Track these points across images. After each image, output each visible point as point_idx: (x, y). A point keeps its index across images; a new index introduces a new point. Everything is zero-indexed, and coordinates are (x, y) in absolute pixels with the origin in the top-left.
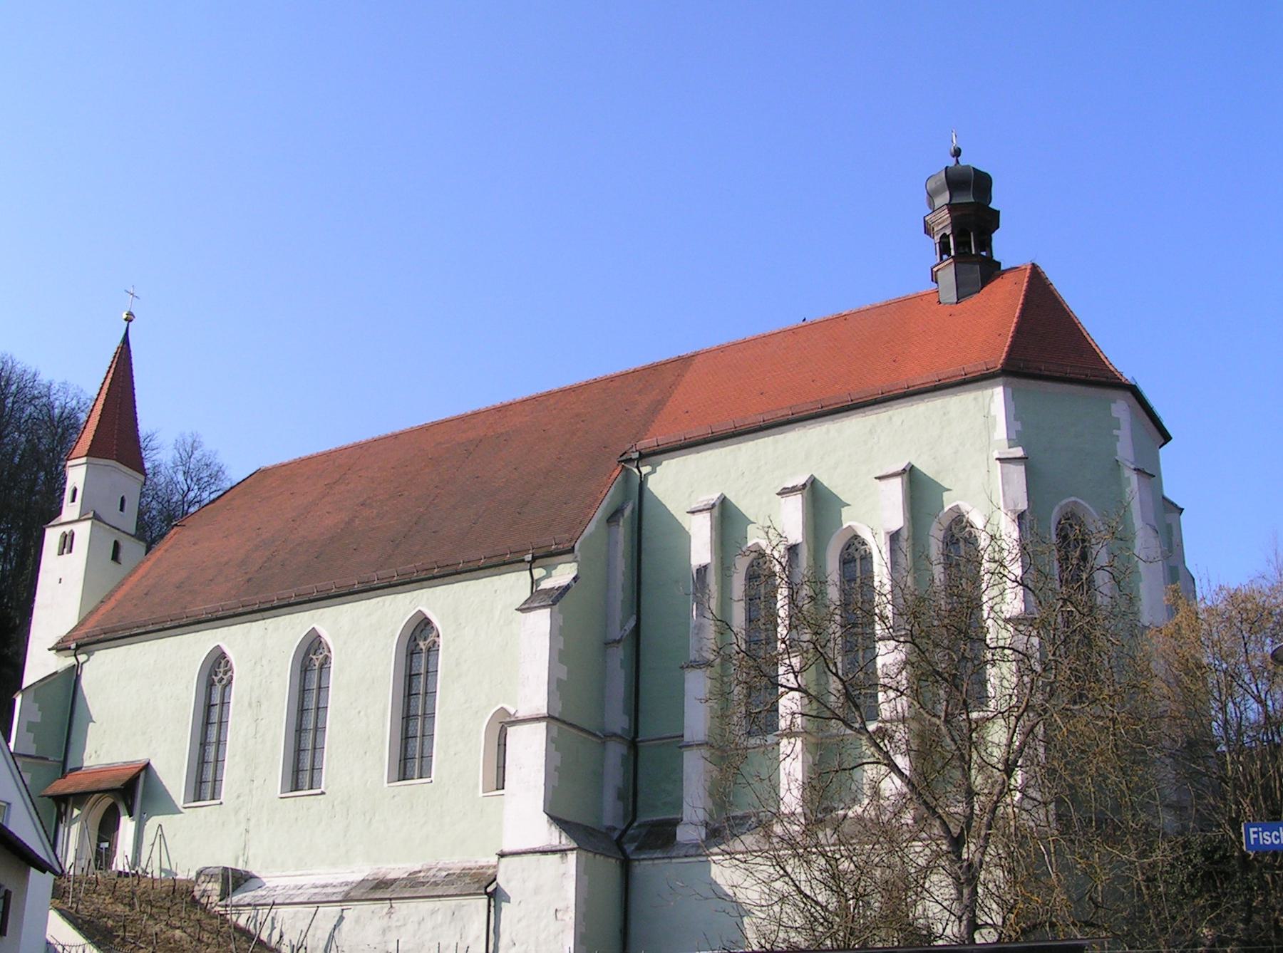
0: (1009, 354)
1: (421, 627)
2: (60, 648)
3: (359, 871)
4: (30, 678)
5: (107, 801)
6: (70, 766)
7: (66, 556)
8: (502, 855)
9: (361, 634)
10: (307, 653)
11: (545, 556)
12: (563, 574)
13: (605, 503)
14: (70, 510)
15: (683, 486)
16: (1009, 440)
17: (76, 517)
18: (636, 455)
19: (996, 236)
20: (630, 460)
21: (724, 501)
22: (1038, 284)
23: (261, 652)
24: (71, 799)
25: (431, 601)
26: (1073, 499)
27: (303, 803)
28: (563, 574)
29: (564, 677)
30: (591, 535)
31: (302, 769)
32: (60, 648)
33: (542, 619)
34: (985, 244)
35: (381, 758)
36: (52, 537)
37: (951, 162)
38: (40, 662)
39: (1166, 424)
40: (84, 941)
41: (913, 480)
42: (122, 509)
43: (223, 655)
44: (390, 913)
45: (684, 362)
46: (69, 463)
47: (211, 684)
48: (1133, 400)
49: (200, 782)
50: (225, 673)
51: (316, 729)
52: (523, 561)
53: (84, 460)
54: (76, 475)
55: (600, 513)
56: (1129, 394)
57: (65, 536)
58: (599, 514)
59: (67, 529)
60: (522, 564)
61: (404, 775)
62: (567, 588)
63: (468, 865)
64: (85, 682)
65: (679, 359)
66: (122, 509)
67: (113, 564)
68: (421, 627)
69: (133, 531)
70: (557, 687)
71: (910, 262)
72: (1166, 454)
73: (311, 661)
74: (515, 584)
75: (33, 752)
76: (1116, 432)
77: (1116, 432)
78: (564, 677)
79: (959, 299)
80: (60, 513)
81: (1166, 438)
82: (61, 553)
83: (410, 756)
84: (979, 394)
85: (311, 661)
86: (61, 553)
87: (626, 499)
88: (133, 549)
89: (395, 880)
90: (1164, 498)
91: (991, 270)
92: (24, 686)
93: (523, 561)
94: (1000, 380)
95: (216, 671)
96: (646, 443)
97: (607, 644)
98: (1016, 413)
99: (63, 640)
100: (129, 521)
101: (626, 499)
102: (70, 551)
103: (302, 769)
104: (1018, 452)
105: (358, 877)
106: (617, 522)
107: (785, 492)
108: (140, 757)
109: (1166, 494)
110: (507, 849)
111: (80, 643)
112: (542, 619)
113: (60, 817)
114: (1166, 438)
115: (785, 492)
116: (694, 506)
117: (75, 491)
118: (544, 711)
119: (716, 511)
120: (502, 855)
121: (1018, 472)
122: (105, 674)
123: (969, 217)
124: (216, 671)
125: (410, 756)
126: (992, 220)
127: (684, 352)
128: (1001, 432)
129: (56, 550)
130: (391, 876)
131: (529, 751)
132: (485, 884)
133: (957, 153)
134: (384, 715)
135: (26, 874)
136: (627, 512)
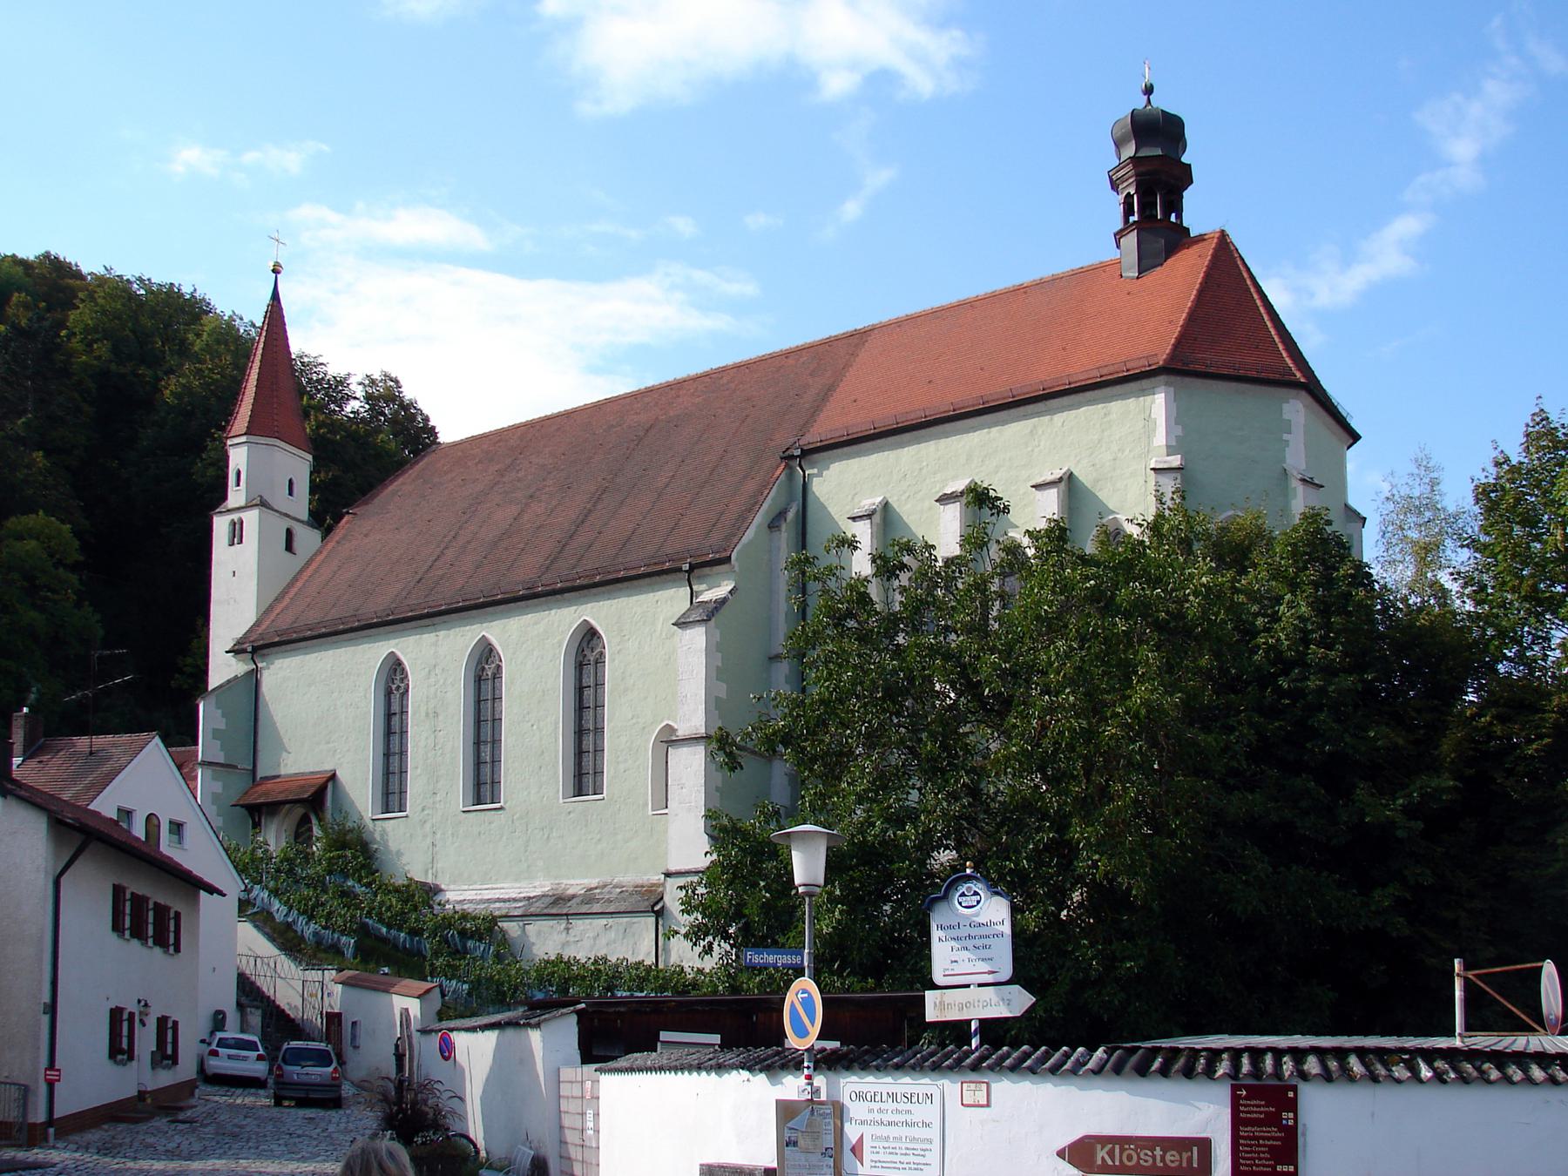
0: (1175, 346)
1: (589, 636)
2: (237, 650)
3: (540, 886)
4: (215, 679)
5: (299, 811)
6: (260, 773)
7: (237, 547)
8: (668, 875)
9: (533, 644)
10: (479, 662)
11: (695, 568)
12: (713, 592)
13: (765, 506)
14: (236, 497)
15: (846, 489)
16: (1168, 447)
17: (243, 503)
18: (798, 452)
19: (1189, 196)
20: (792, 457)
21: (886, 506)
22: (1225, 255)
23: (436, 659)
24: (264, 809)
25: (598, 612)
26: (1231, 513)
27: (483, 820)
28: (713, 592)
29: (723, 695)
30: (751, 543)
31: (484, 785)
32: (237, 650)
33: (697, 638)
34: (1175, 205)
35: (556, 773)
36: (221, 525)
37: (1140, 102)
38: (222, 667)
39: (1354, 424)
40: (277, 952)
41: (1069, 485)
42: (291, 493)
43: (399, 663)
44: (567, 929)
45: (858, 338)
46: (229, 442)
47: (389, 693)
48: (1309, 399)
49: (387, 794)
50: (402, 680)
51: (494, 742)
52: (680, 570)
53: (243, 439)
54: (238, 457)
55: (760, 519)
56: (1304, 393)
57: (233, 523)
58: (758, 519)
59: (235, 516)
60: (680, 575)
61: (579, 791)
62: (723, 602)
63: (640, 882)
64: (266, 688)
65: (852, 335)
66: (291, 493)
67: (288, 554)
68: (589, 636)
69: (305, 516)
70: (714, 704)
71: (1086, 225)
72: (1353, 456)
73: (485, 671)
74: (673, 599)
75: (222, 761)
76: (1285, 437)
77: (1285, 437)
78: (723, 695)
79: (1142, 270)
80: (225, 498)
81: (1355, 437)
82: (232, 544)
83: (584, 774)
84: (1099, 408)
85: (485, 671)
86: (232, 544)
87: (791, 500)
88: (308, 539)
89: (574, 896)
90: (1346, 506)
91: (1178, 238)
92: (210, 688)
93: (680, 570)
94: (1162, 378)
95: (394, 675)
96: (812, 437)
97: (776, 658)
98: (1177, 418)
99: (239, 642)
100: (300, 505)
101: (791, 500)
102: (241, 542)
103: (484, 785)
104: (1175, 461)
105: (538, 892)
106: (778, 528)
107: (944, 499)
108: (328, 767)
109: (1353, 502)
110: (673, 868)
111: (255, 647)
112: (697, 638)
113: (256, 825)
114: (1355, 437)
115: (944, 499)
116: (857, 512)
117: (239, 473)
118: (702, 731)
119: (877, 518)
120: (668, 875)
121: (1169, 485)
122: (286, 679)
123: (1156, 163)
124: (394, 675)
125: (584, 774)
126: (1184, 176)
127: (860, 324)
128: (1160, 439)
129: (226, 541)
130: (571, 892)
131: (690, 766)
132: (653, 900)
133: (1149, 90)
134: (556, 728)
135: (196, 898)
136: (791, 515)
